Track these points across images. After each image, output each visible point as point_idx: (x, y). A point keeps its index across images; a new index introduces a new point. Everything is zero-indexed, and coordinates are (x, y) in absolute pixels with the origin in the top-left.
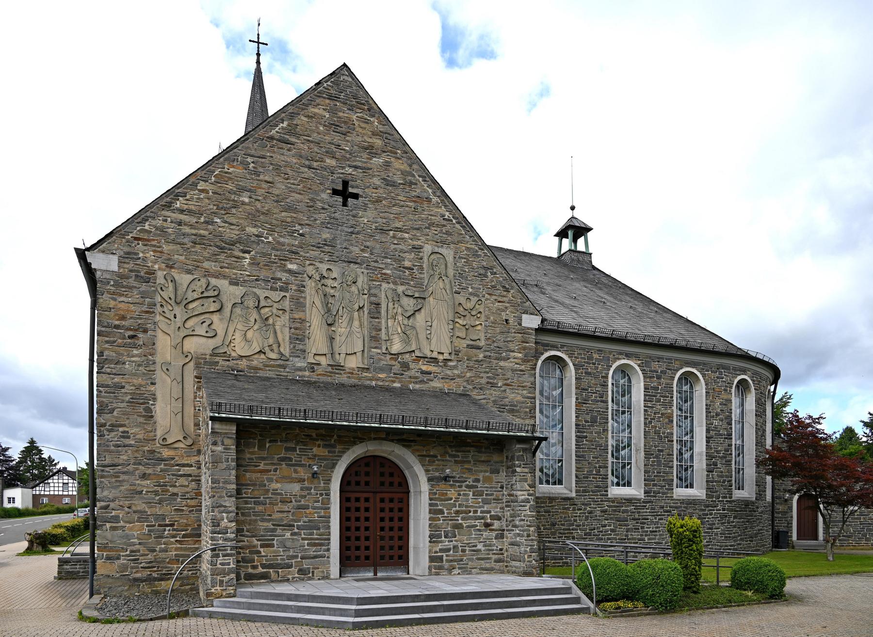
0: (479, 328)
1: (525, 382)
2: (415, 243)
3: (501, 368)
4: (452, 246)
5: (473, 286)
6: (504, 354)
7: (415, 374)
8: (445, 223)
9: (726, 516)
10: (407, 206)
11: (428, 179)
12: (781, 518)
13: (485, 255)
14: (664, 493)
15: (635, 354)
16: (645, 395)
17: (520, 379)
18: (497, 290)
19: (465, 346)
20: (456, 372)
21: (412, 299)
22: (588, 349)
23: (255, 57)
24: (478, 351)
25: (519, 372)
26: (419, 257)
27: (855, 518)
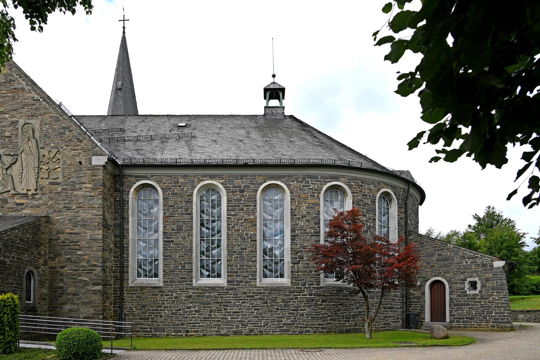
0: (59, 170)
1: (94, 204)
2: (13, 119)
3: (75, 196)
4: (40, 117)
5: (54, 142)
6: (78, 186)
7: (12, 206)
8: (34, 102)
9: (313, 300)
10: (8, 96)
11: (22, 76)
12: (416, 302)
13: (63, 119)
14: (247, 282)
15: (219, 176)
16: (228, 206)
17: (90, 202)
18: (73, 142)
19: (48, 183)
20: (41, 202)
21: (9, 157)
22: (174, 176)
23: (122, 29)
24: (57, 186)
25: (89, 198)
26: (16, 128)
27: (476, 301)
